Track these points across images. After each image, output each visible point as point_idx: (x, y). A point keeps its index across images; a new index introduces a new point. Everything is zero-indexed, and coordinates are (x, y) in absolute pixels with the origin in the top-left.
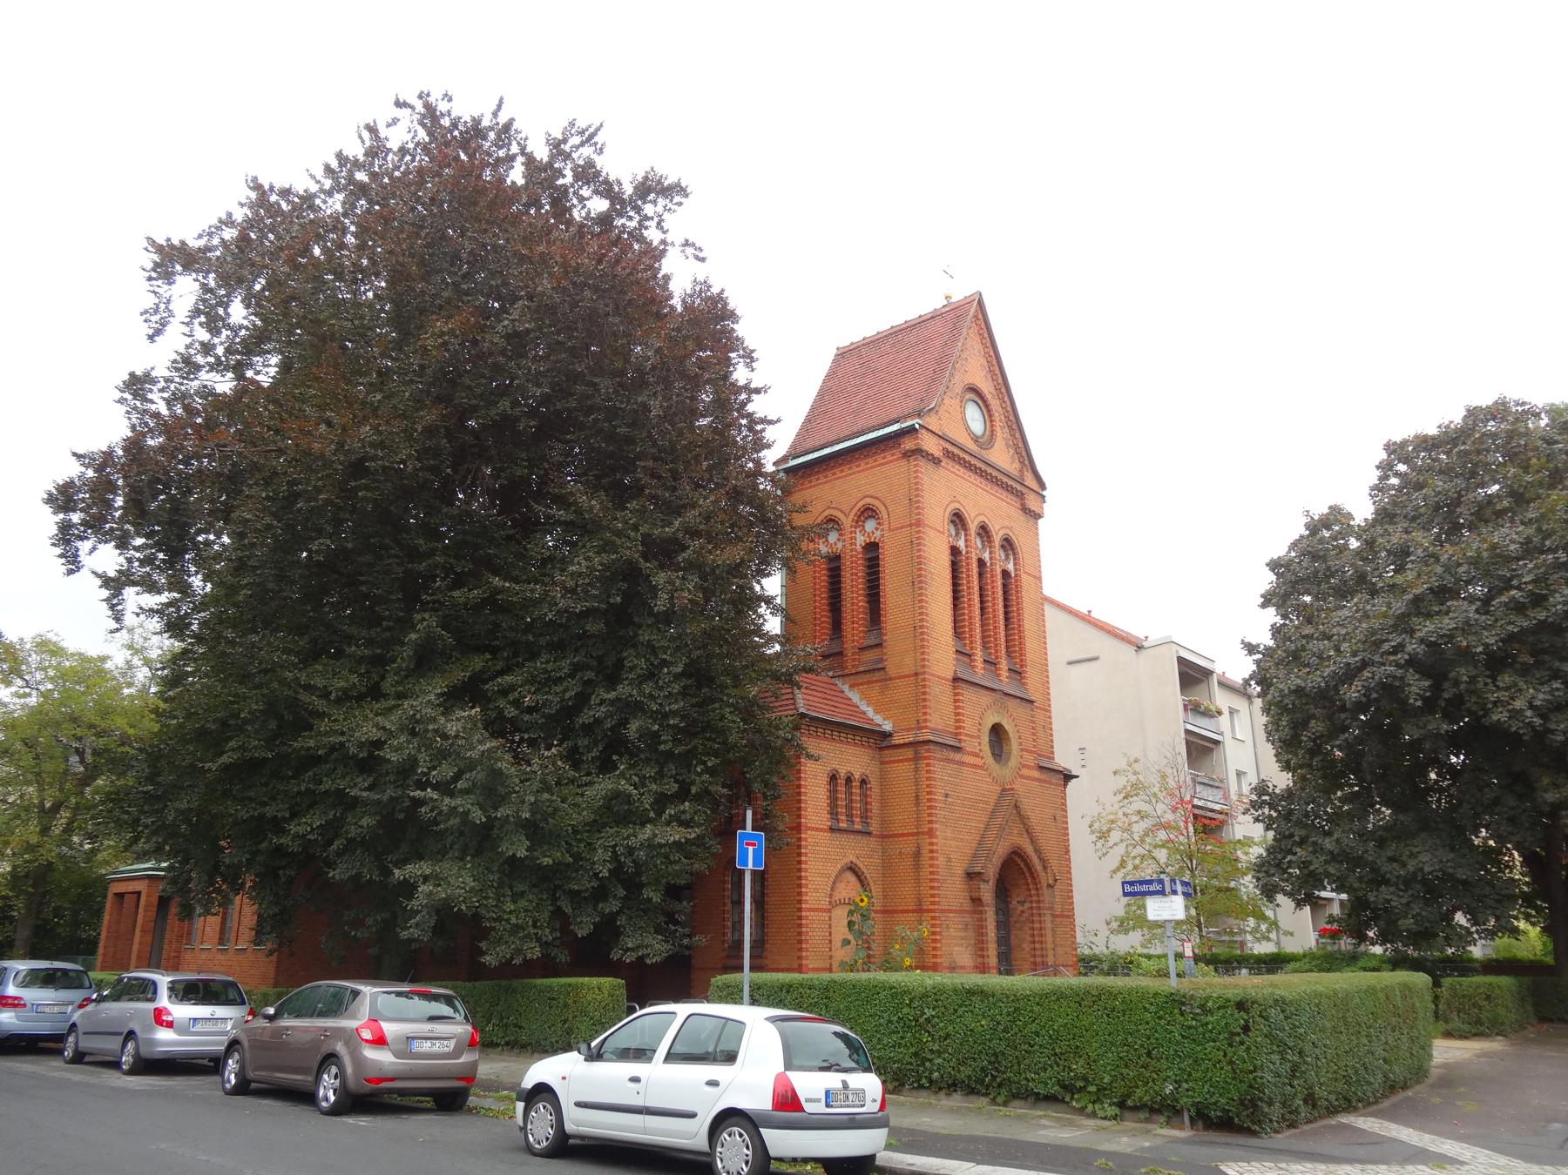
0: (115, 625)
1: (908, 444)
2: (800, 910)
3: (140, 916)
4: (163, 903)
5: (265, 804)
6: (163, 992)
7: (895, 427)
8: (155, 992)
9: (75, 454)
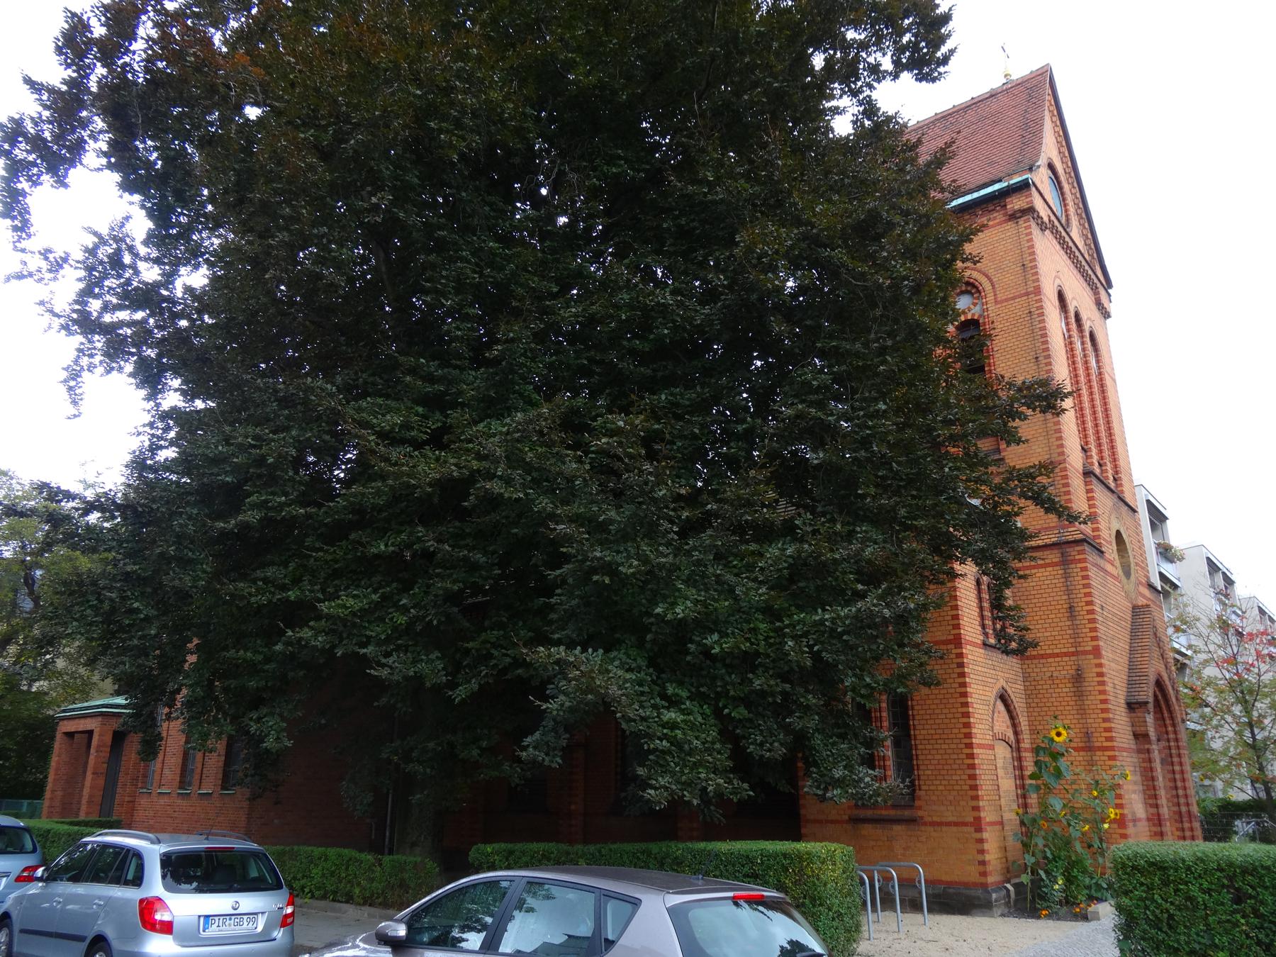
0: (72, 410)
1: (1016, 203)
2: (970, 746)
3: (92, 757)
4: (119, 738)
5: (284, 588)
6: (154, 871)
7: (997, 187)
8: (140, 868)
9: (29, 81)
